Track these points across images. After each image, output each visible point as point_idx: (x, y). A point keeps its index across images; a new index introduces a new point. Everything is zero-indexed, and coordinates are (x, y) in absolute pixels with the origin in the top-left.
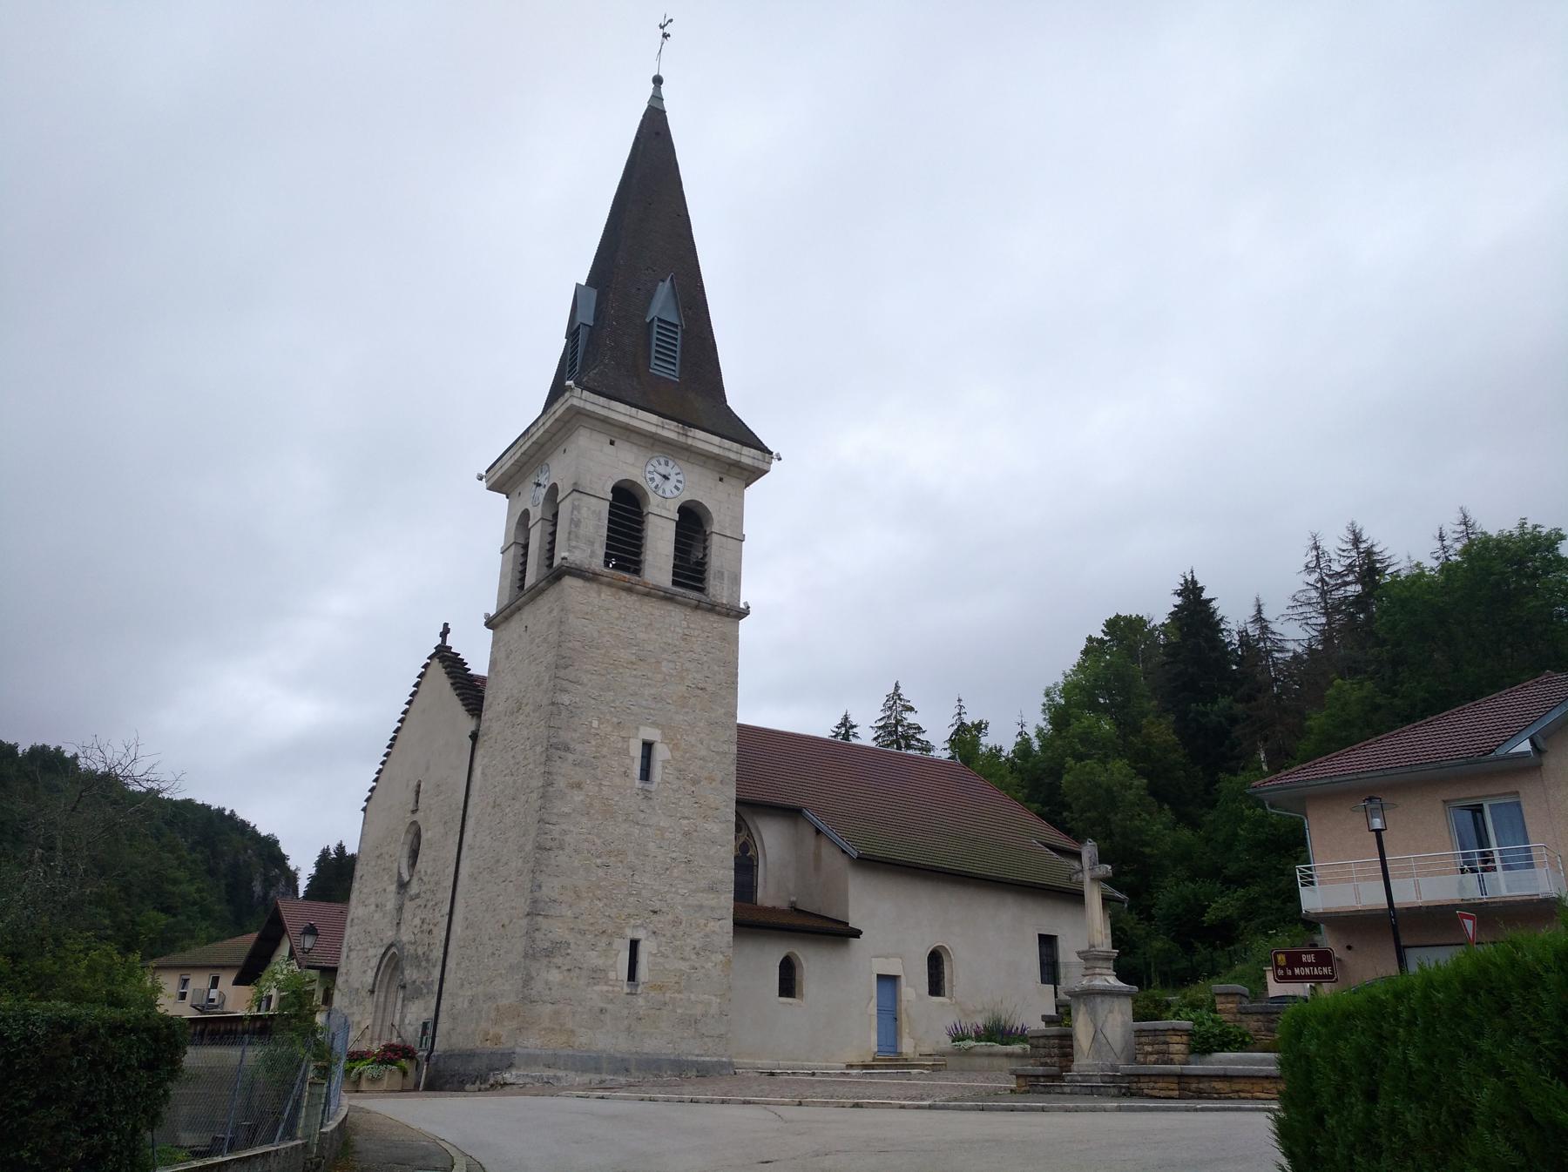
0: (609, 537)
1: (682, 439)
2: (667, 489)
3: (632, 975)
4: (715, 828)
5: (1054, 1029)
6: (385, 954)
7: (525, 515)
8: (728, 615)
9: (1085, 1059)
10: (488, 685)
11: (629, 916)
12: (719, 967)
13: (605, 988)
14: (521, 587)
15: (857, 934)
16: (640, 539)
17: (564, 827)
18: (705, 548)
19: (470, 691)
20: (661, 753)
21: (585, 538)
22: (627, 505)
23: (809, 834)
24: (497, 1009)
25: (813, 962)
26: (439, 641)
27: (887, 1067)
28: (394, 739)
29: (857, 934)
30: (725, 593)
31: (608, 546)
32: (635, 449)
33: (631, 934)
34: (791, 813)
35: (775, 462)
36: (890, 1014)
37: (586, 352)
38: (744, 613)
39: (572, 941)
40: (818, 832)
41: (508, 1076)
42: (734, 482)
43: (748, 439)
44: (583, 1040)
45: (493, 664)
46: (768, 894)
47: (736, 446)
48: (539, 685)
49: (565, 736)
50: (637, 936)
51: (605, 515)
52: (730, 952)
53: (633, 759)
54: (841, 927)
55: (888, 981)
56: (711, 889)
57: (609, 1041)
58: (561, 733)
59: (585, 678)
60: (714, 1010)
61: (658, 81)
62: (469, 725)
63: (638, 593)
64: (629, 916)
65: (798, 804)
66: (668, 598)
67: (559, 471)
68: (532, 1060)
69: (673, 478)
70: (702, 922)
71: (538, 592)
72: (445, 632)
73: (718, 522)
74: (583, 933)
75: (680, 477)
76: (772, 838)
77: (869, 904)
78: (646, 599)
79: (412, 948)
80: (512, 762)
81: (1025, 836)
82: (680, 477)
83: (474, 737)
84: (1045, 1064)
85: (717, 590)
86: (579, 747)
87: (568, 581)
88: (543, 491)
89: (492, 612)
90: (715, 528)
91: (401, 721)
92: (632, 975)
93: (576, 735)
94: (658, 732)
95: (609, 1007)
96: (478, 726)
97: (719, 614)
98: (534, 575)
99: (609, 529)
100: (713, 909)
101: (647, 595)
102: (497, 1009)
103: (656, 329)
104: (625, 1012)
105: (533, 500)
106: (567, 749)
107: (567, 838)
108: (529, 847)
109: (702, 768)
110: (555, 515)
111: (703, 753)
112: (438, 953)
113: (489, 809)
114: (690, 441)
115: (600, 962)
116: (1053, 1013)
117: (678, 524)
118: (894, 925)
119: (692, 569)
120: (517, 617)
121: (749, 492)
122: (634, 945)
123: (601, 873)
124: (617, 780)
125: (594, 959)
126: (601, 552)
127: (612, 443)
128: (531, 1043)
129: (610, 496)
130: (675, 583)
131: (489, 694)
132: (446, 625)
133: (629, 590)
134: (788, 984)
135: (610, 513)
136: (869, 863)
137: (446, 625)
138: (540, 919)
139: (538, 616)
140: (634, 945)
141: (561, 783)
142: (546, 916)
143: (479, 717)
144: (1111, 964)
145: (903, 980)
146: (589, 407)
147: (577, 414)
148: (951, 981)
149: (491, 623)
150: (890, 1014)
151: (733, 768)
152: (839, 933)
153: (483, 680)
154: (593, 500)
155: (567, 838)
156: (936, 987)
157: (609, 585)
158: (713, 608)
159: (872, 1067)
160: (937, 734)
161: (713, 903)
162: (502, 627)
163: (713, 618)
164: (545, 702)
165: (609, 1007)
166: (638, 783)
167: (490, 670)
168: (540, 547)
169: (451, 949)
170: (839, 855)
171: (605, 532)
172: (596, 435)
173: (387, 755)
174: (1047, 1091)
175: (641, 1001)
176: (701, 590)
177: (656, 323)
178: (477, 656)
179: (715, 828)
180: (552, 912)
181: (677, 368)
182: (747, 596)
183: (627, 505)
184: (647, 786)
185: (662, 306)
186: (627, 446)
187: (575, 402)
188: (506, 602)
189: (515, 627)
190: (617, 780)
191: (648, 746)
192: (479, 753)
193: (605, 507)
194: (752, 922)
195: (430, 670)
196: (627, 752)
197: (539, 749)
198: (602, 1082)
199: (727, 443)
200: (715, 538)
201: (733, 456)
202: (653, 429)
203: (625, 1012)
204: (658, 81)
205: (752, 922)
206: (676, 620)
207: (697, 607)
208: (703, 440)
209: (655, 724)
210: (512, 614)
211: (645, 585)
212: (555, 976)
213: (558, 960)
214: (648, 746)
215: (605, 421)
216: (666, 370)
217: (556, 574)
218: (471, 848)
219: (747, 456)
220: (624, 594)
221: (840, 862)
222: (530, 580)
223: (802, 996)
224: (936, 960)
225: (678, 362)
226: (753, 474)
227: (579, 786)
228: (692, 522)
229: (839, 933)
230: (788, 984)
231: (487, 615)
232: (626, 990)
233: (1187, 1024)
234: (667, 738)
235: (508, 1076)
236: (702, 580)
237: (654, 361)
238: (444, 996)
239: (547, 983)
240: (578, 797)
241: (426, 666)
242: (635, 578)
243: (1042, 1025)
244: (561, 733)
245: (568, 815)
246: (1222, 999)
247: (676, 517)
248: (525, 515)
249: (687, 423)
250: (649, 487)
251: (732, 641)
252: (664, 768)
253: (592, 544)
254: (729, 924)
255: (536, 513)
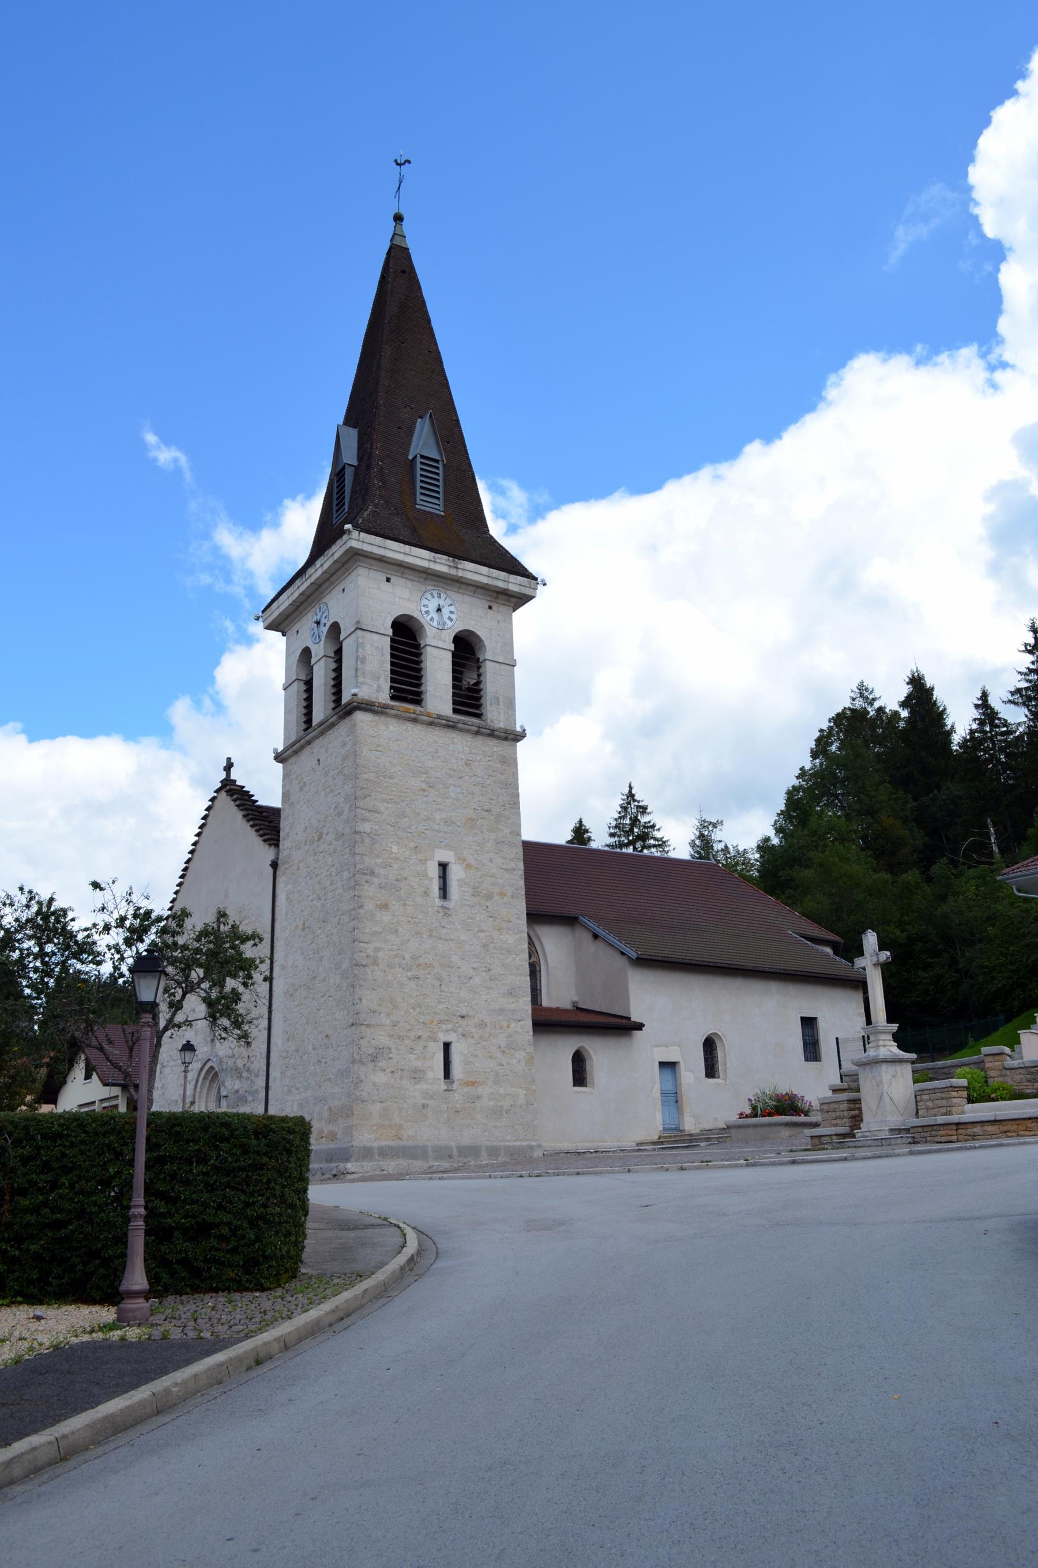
0: (392, 672)
1: (453, 572)
2: (441, 618)
3: (447, 1074)
4: (510, 939)
5: (844, 1096)
6: (202, 1068)
7: (306, 653)
8: (506, 739)
9: (873, 1123)
10: (283, 815)
11: (441, 1022)
12: (523, 1062)
13: (425, 1086)
14: (309, 721)
15: (639, 1027)
16: (419, 670)
17: (378, 945)
18: (479, 675)
19: (266, 822)
20: (456, 873)
21: (370, 673)
22: (406, 636)
23: (587, 937)
24: (330, 1109)
25: (601, 1053)
26: (223, 775)
27: (675, 1142)
28: (185, 869)
29: (639, 1027)
30: (502, 717)
31: (392, 680)
32: (409, 584)
33: (444, 1038)
34: (569, 921)
35: (540, 587)
36: (673, 1099)
37: (353, 492)
38: (520, 736)
39: (393, 1046)
40: (596, 936)
41: (350, 1166)
42: (503, 609)
43: (512, 566)
44: (411, 1132)
45: (286, 796)
46: (559, 995)
47: (503, 575)
48: (339, 814)
49: (369, 862)
50: (448, 1039)
51: (387, 651)
52: (531, 1049)
53: (431, 879)
54: (624, 1021)
55: (668, 1066)
56: (511, 993)
57: (429, 1133)
58: (367, 859)
59: (382, 807)
60: (521, 1100)
61: (398, 218)
62: (270, 854)
63: (423, 723)
64: (441, 1022)
65: (573, 913)
66: (451, 726)
67: (337, 607)
68: (367, 1153)
69: (445, 611)
70: (505, 1024)
71: (327, 726)
72: (229, 766)
73: (490, 651)
74: (401, 1038)
75: (452, 608)
76: (555, 944)
77: (649, 997)
78: (430, 729)
79: (230, 1062)
80: (317, 887)
81: (787, 928)
82: (452, 608)
83: (274, 865)
84: (836, 1125)
85: (493, 715)
86: (382, 871)
87: (359, 716)
88: (325, 630)
89: (280, 748)
90: (488, 655)
91: (192, 852)
92: (447, 1074)
93: (379, 861)
94: (452, 854)
95: (430, 1102)
96: (278, 854)
97: (498, 738)
98: (319, 709)
99: (392, 664)
100: (514, 1011)
101: (431, 724)
102: (330, 1109)
103: (419, 466)
104: (444, 1107)
105: (308, 633)
106: (372, 873)
107: (380, 954)
108: (346, 964)
109: (493, 884)
110: (339, 652)
111: (494, 871)
112: (260, 1064)
113: (299, 931)
114: (460, 574)
115: (419, 1064)
116: (838, 1081)
117: (455, 655)
118: (672, 1012)
119: (468, 699)
120: (306, 751)
121: (518, 744)
122: (447, 1046)
123: (413, 984)
124: (420, 900)
125: (413, 1061)
126: (386, 685)
127: (388, 580)
128: (364, 1138)
129: (390, 632)
130: (455, 711)
131: (284, 825)
132: (229, 759)
133: (415, 721)
134: (580, 1077)
135: (392, 648)
136: (644, 962)
137: (229, 759)
138: (363, 1028)
139: (330, 748)
140: (447, 1046)
141: (369, 906)
142: (368, 1026)
143: (277, 846)
144: (890, 1037)
145: (682, 1066)
146: (366, 548)
147: (355, 556)
148: (725, 1064)
149: (279, 758)
150: (673, 1099)
151: (522, 883)
152: (622, 1027)
153: (276, 812)
154: (376, 637)
155: (380, 954)
156: (711, 1071)
157: (396, 717)
158: (492, 734)
159: (662, 1143)
160: (678, 840)
161: (513, 1006)
162: (293, 760)
163: (493, 742)
164: (347, 831)
165: (430, 1102)
166: (438, 902)
167: (284, 801)
168: (326, 684)
169: (272, 1060)
170: (617, 956)
171: (388, 667)
172: (373, 574)
173: (180, 885)
174: (841, 1146)
175: (457, 1096)
176: (479, 716)
177: (419, 460)
178: (267, 788)
179: (510, 939)
180: (373, 1022)
181: (441, 502)
182: (521, 720)
183: (406, 636)
184: (446, 904)
185: (423, 442)
186: (402, 581)
187: (354, 544)
188: (293, 738)
189: (306, 759)
190: (420, 900)
191: (443, 866)
192: (280, 880)
193: (386, 642)
194: (547, 1023)
195: (217, 802)
196: (424, 874)
197: (346, 875)
198: (430, 1167)
199: (495, 573)
200: (488, 663)
201: (501, 585)
202: (425, 564)
203: (444, 1107)
204: (398, 218)
205: (547, 1023)
206: (461, 746)
207: (477, 733)
208: (472, 571)
209: (449, 847)
210: (302, 748)
211: (429, 715)
212: (380, 1078)
213: (382, 1064)
214: (443, 866)
215: (381, 560)
216: (430, 504)
217: (344, 709)
218: (283, 968)
219: (514, 583)
220: (409, 726)
221: (621, 962)
222: (318, 716)
223: (593, 1085)
224: (710, 1045)
225: (441, 496)
226: (521, 599)
227: (385, 907)
228: (466, 650)
229: (622, 1027)
230: (580, 1077)
231: (275, 750)
232: (444, 1087)
233: (964, 1082)
234: (461, 859)
235: (350, 1166)
236: (478, 707)
237: (419, 497)
238: (270, 1102)
239: (374, 1084)
240: (386, 917)
241: (213, 800)
242: (418, 709)
243: (830, 1093)
244: (367, 859)
245: (376, 933)
246: (990, 1058)
247: (452, 647)
248: (306, 653)
249: (457, 554)
250: (425, 620)
251: (511, 763)
252: (460, 886)
253: (378, 678)
254: (529, 1023)
255: (319, 650)
